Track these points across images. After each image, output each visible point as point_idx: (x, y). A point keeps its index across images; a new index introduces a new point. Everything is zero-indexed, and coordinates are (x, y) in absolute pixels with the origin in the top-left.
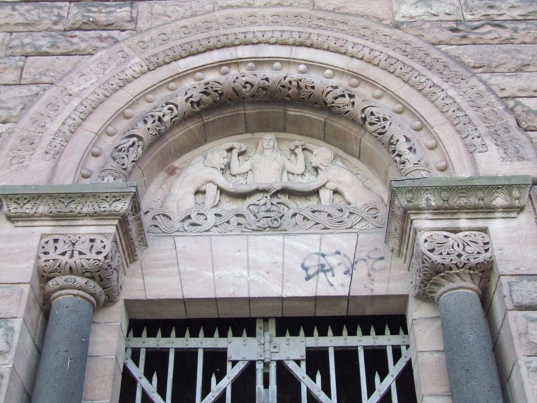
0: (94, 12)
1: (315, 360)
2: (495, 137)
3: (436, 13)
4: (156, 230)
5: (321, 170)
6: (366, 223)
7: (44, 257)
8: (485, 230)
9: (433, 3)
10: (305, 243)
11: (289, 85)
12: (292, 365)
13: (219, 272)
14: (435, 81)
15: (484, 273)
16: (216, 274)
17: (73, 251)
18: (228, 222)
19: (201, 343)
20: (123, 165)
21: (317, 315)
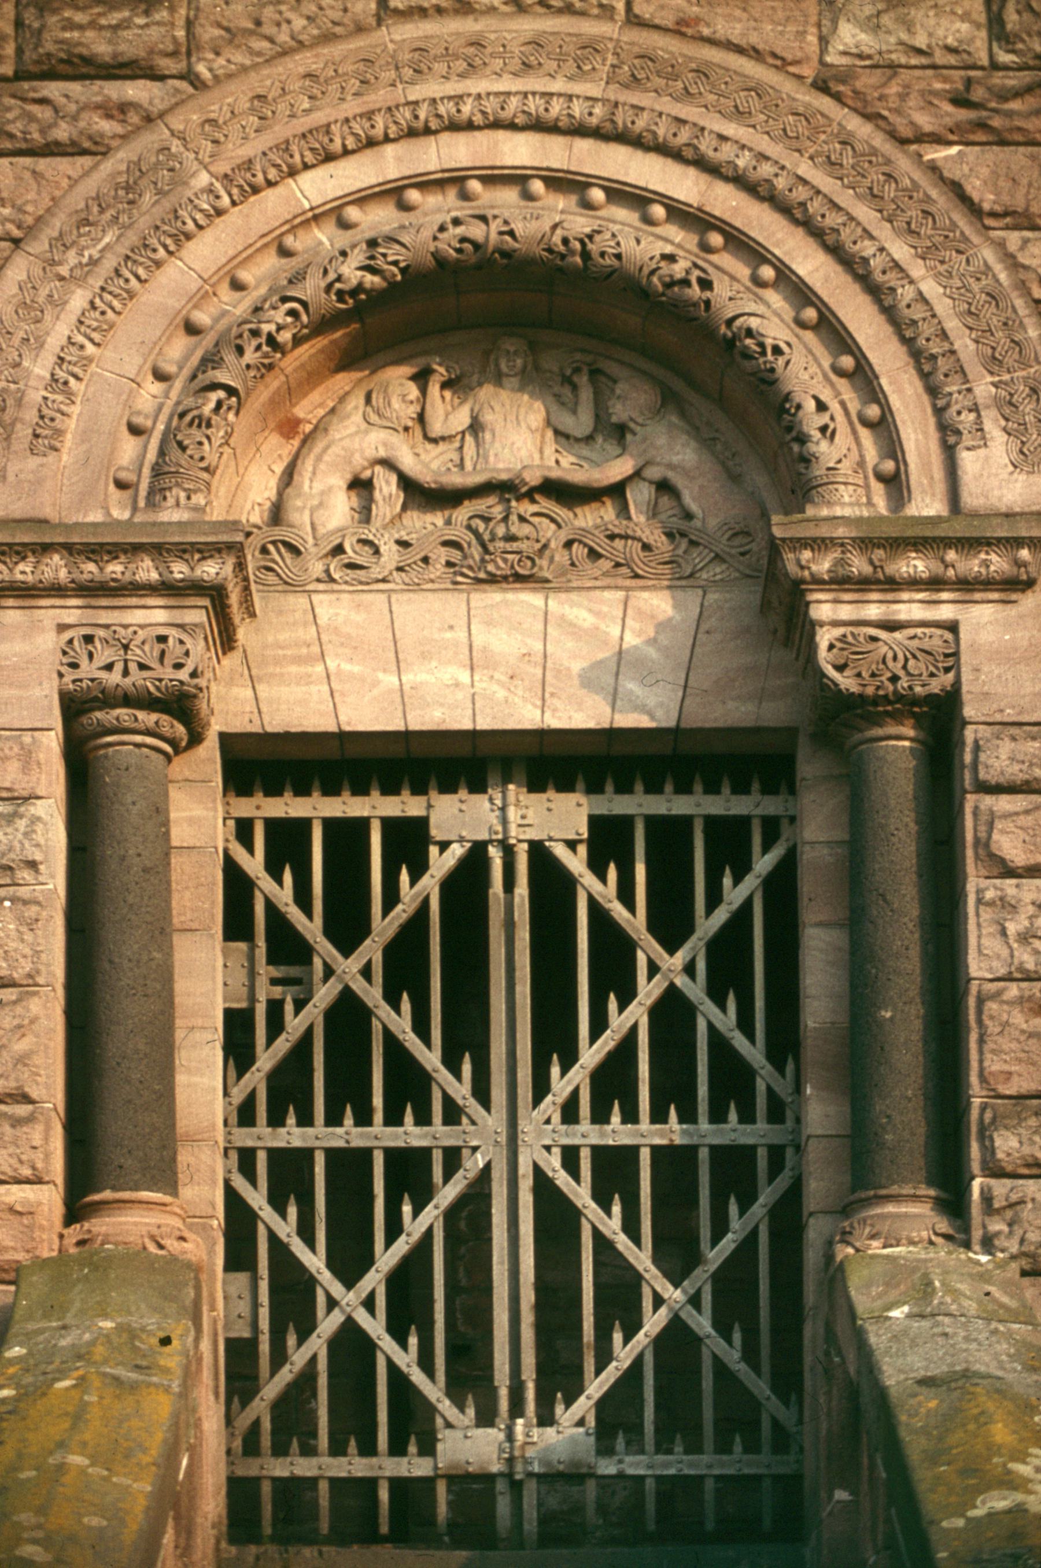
0: (81, 27)
1: (607, 842)
2: (1007, 411)
3: (924, 47)
4: (271, 578)
5: (634, 434)
6: (724, 566)
7: (70, 676)
8: (953, 627)
9: (916, 14)
10: (590, 610)
11: (562, 248)
12: (560, 851)
13: (411, 677)
14: (896, 257)
15: (940, 718)
16: (404, 679)
17: (126, 661)
18: (426, 560)
19: (376, 807)
20: (202, 459)
21: (616, 725)
